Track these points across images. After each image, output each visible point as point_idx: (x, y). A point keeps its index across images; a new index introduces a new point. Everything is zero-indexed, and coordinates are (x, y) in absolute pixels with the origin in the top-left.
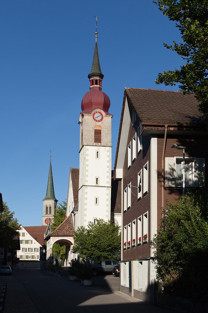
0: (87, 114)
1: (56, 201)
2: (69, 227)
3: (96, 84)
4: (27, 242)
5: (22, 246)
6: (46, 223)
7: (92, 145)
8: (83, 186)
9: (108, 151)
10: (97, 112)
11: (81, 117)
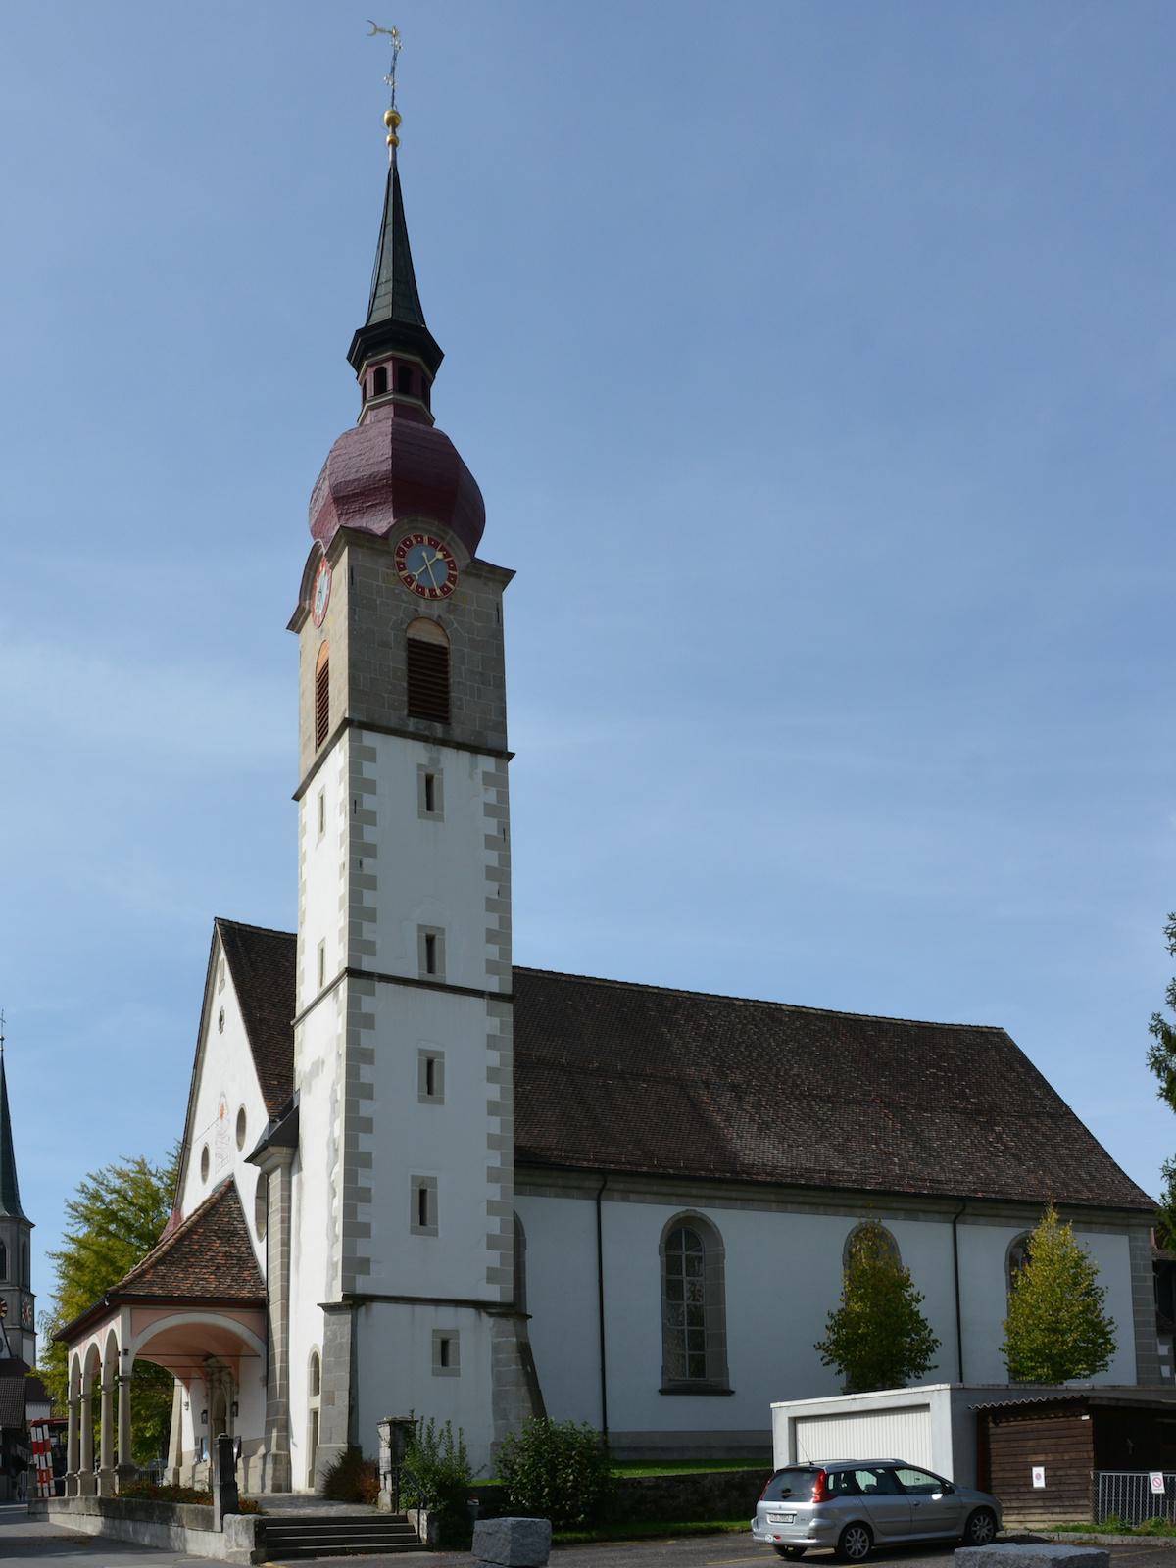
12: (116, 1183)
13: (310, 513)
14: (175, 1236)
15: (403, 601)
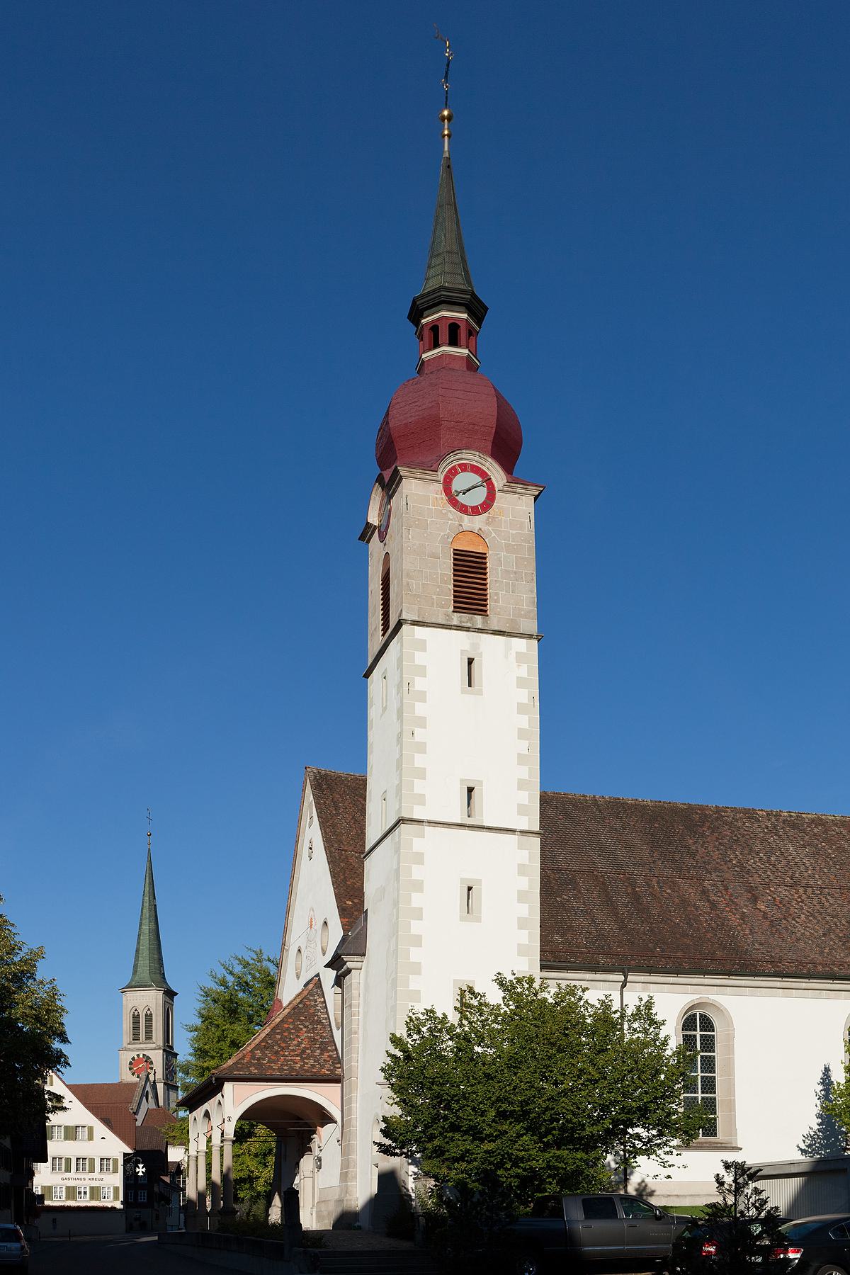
0: (416, 472)
1: (170, 994)
2: (313, 1040)
3: (454, 342)
4: (71, 1133)
5: (55, 1147)
6: (133, 1074)
7: (443, 622)
8: (401, 821)
9: (520, 658)
10: (464, 468)
11: (377, 496)
12: (238, 969)
13: (377, 447)
14: (482, 456)
15: (450, 519)
